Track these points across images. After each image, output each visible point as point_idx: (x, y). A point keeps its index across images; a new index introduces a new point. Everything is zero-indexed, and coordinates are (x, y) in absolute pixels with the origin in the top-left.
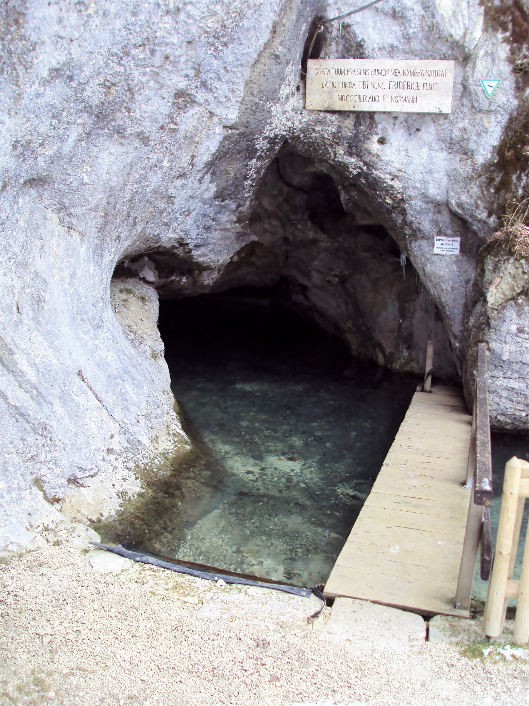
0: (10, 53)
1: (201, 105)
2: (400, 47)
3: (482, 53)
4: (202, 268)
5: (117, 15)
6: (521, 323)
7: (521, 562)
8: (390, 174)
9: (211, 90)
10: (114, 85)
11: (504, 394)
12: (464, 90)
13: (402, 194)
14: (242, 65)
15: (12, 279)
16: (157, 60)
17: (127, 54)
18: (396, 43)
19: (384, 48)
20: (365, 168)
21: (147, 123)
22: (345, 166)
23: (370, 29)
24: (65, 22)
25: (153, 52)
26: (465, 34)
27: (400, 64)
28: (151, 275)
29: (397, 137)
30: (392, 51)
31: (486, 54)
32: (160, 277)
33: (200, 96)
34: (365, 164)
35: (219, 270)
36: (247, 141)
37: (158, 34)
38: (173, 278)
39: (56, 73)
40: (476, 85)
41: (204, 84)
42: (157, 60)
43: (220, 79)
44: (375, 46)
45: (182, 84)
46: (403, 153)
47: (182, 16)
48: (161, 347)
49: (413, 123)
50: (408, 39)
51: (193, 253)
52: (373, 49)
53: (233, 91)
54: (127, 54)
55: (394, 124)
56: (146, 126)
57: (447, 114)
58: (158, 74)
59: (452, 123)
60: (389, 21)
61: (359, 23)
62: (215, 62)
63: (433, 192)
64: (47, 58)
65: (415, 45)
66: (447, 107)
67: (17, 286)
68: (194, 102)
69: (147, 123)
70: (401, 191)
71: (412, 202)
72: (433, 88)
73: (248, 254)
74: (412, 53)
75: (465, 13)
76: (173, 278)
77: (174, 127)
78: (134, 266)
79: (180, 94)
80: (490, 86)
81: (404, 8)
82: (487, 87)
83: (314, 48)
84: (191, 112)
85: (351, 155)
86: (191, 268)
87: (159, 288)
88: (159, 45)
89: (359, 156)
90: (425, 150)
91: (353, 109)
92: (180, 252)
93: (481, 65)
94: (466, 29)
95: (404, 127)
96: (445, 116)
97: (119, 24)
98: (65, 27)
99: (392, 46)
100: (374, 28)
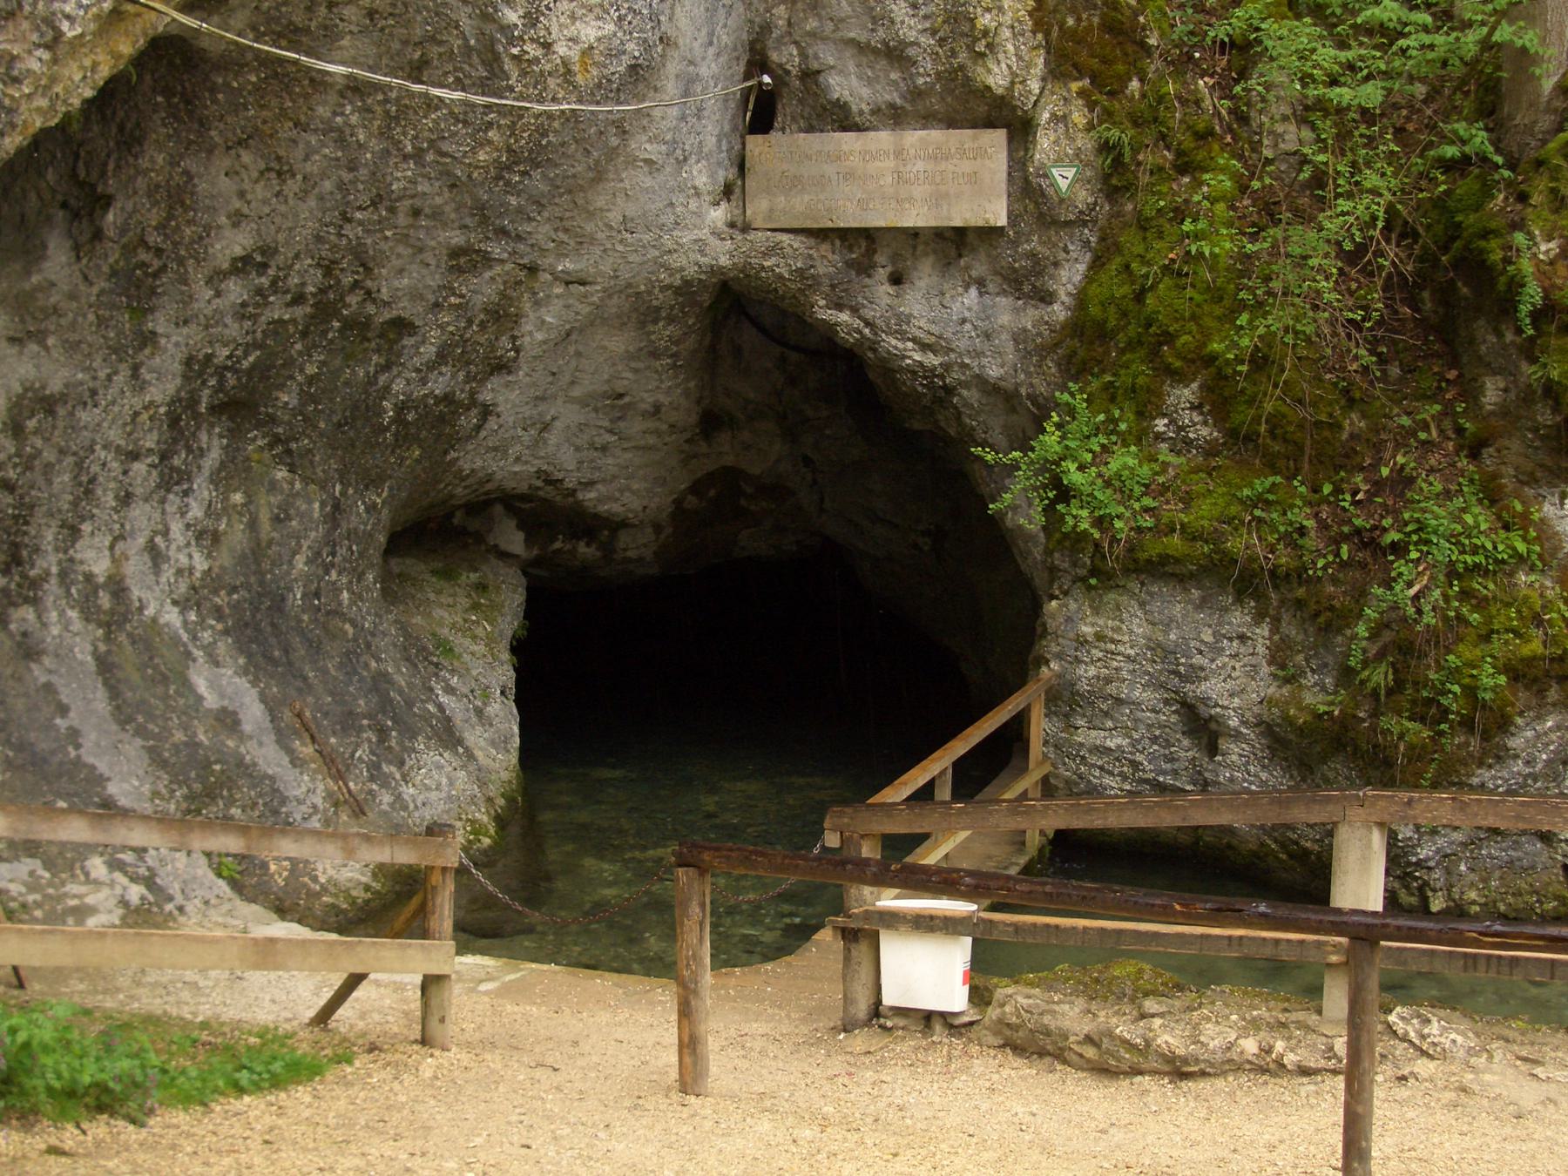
0: (175, 244)
1: (502, 261)
2: (908, 107)
3: (1046, 115)
4: (617, 525)
5: (324, 176)
6: (1101, 622)
7: (1018, 1049)
8: (914, 340)
9: (518, 236)
10: (333, 262)
11: (1093, 759)
12: (1027, 189)
13: (942, 377)
14: (570, 192)
15: (190, 557)
16: (402, 220)
17: (349, 220)
18: (899, 101)
19: (879, 110)
20: (867, 331)
21: (405, 303)
22: (831, 327)
23: (848, 84)
24: (249, 197)
25: (392, 210)
26: (1013, 83)
27: (913, 138)
28: (513, 540)
29: (925, 276)
30: (895, 117)
31: (1055, 118)
32: (529, 542)
33: (496, 249)
34: (867, 324)
35: (658, 528)
36: (628, 296)
37: (394, 187)
38: (557, 545)
39: (242, 265)
40: (1039, 176)
41: (502, 232)
42: (402, 220)
43: (530, 219)
44: (864, 106)
45: (457, 238)
46: (936, 301)
47: (430, 157)
48: (511, 684)
49: (954, 244)
50: (916, 94)
51: (580, 496)
52: (861, 112)
53: (566, 230)
54: (349, 220)
55: (915, 248)
56: (404, 308)
57: (1002, 228)
58: (407, 235)
59: (1015, 243)
60: (883, 63)
61: (832, 67)
62: (513, 201)
63: (994, 372)
64: (232, 244)
65: (935, 104)
66: (997, 213)
67: (198, 567)
68: (488, 260)
69: (405, 303)
70: (939, 371)
71: (965, 393)
72: (942, 179)
73: (714, 500)
74: (928, 119)
75: (1010, 47)
76: (557, 545)
77: (458, 301)
78: (474, 524)
79: (455, 253)
80: (1063, 178)
81: (904, 44)
82: (1059, 179)
83: (761, 114)
84: (488, 275)
85: (839, 307)
86: (586, 525)
87: (526, 568)
88: (399, 199)
89: (855, 310)
90: (973, 292)
91: (830, 225)
92: (549, 492)
93: (1045, 143)
94: (1014, 74)
95: (935, 252)
96: (1000, 231)
97: (328, 185)
98: (249, 203)
99: (892, 106)
100: (860, 78)
